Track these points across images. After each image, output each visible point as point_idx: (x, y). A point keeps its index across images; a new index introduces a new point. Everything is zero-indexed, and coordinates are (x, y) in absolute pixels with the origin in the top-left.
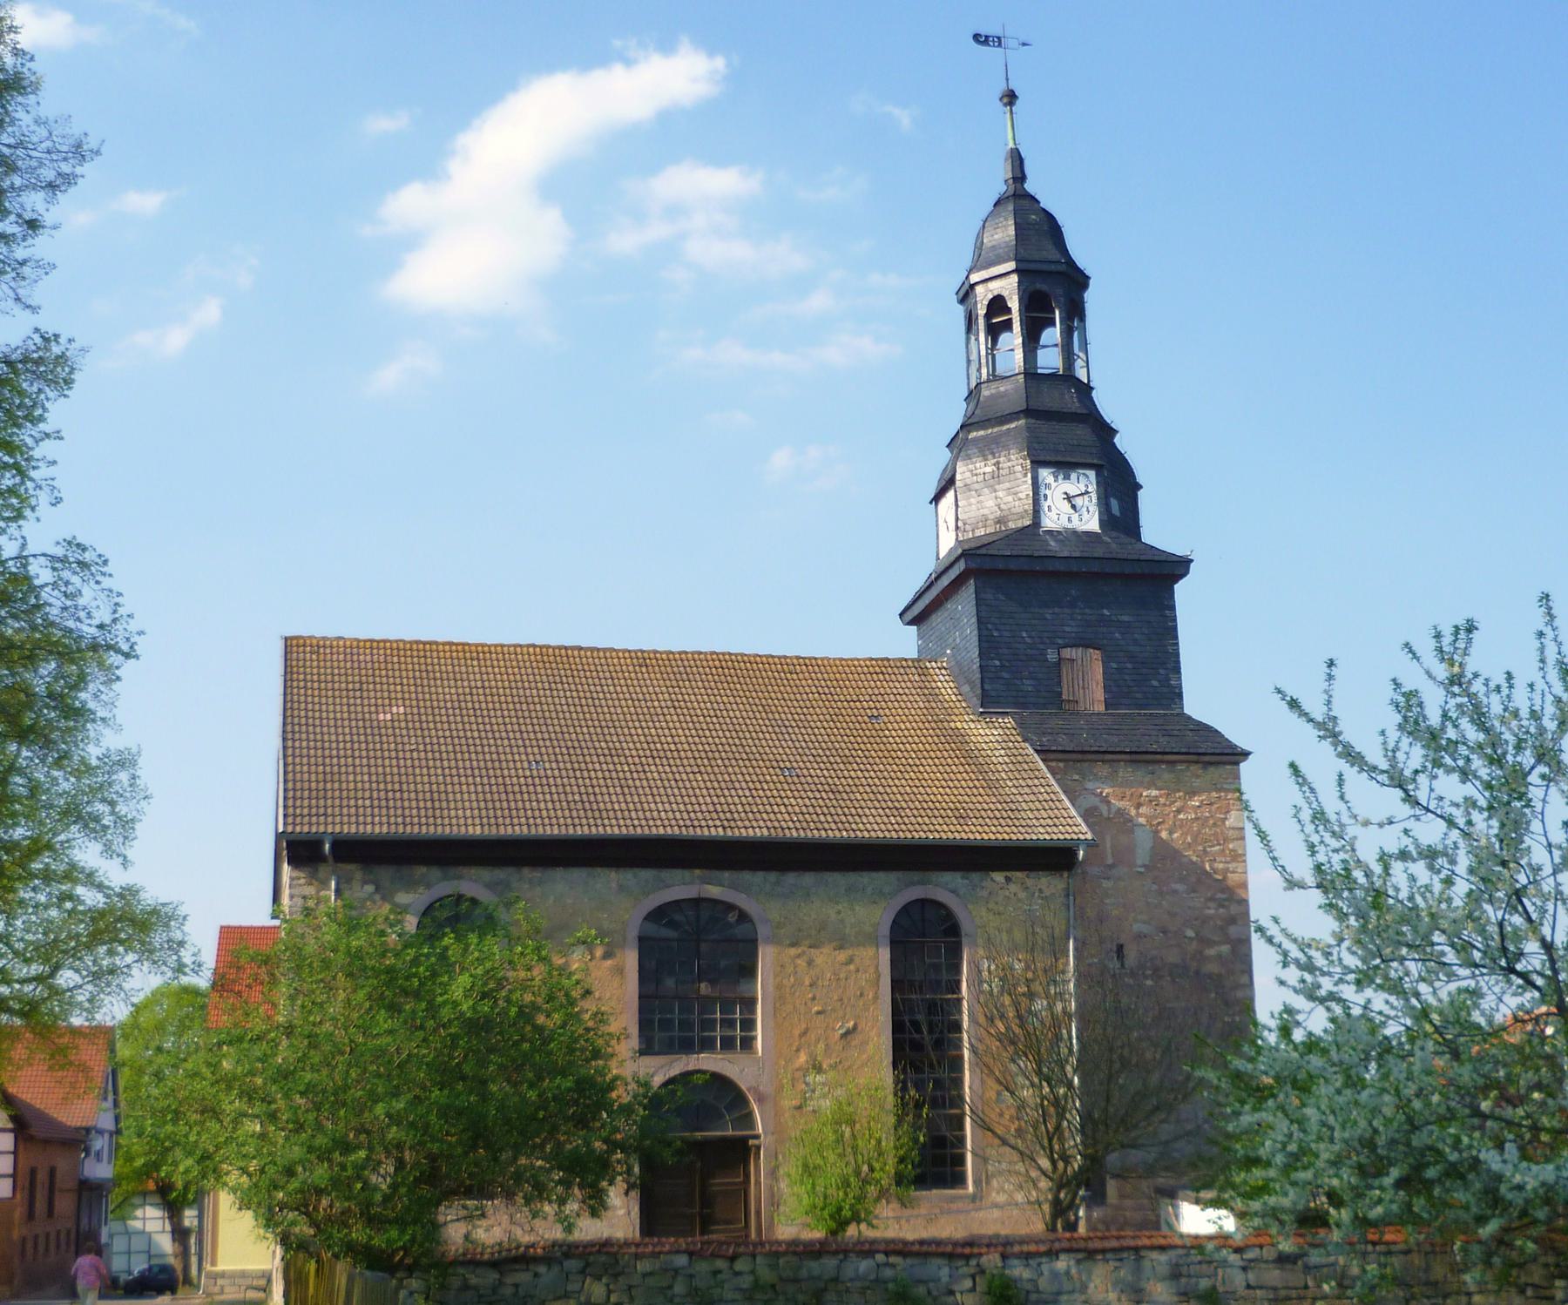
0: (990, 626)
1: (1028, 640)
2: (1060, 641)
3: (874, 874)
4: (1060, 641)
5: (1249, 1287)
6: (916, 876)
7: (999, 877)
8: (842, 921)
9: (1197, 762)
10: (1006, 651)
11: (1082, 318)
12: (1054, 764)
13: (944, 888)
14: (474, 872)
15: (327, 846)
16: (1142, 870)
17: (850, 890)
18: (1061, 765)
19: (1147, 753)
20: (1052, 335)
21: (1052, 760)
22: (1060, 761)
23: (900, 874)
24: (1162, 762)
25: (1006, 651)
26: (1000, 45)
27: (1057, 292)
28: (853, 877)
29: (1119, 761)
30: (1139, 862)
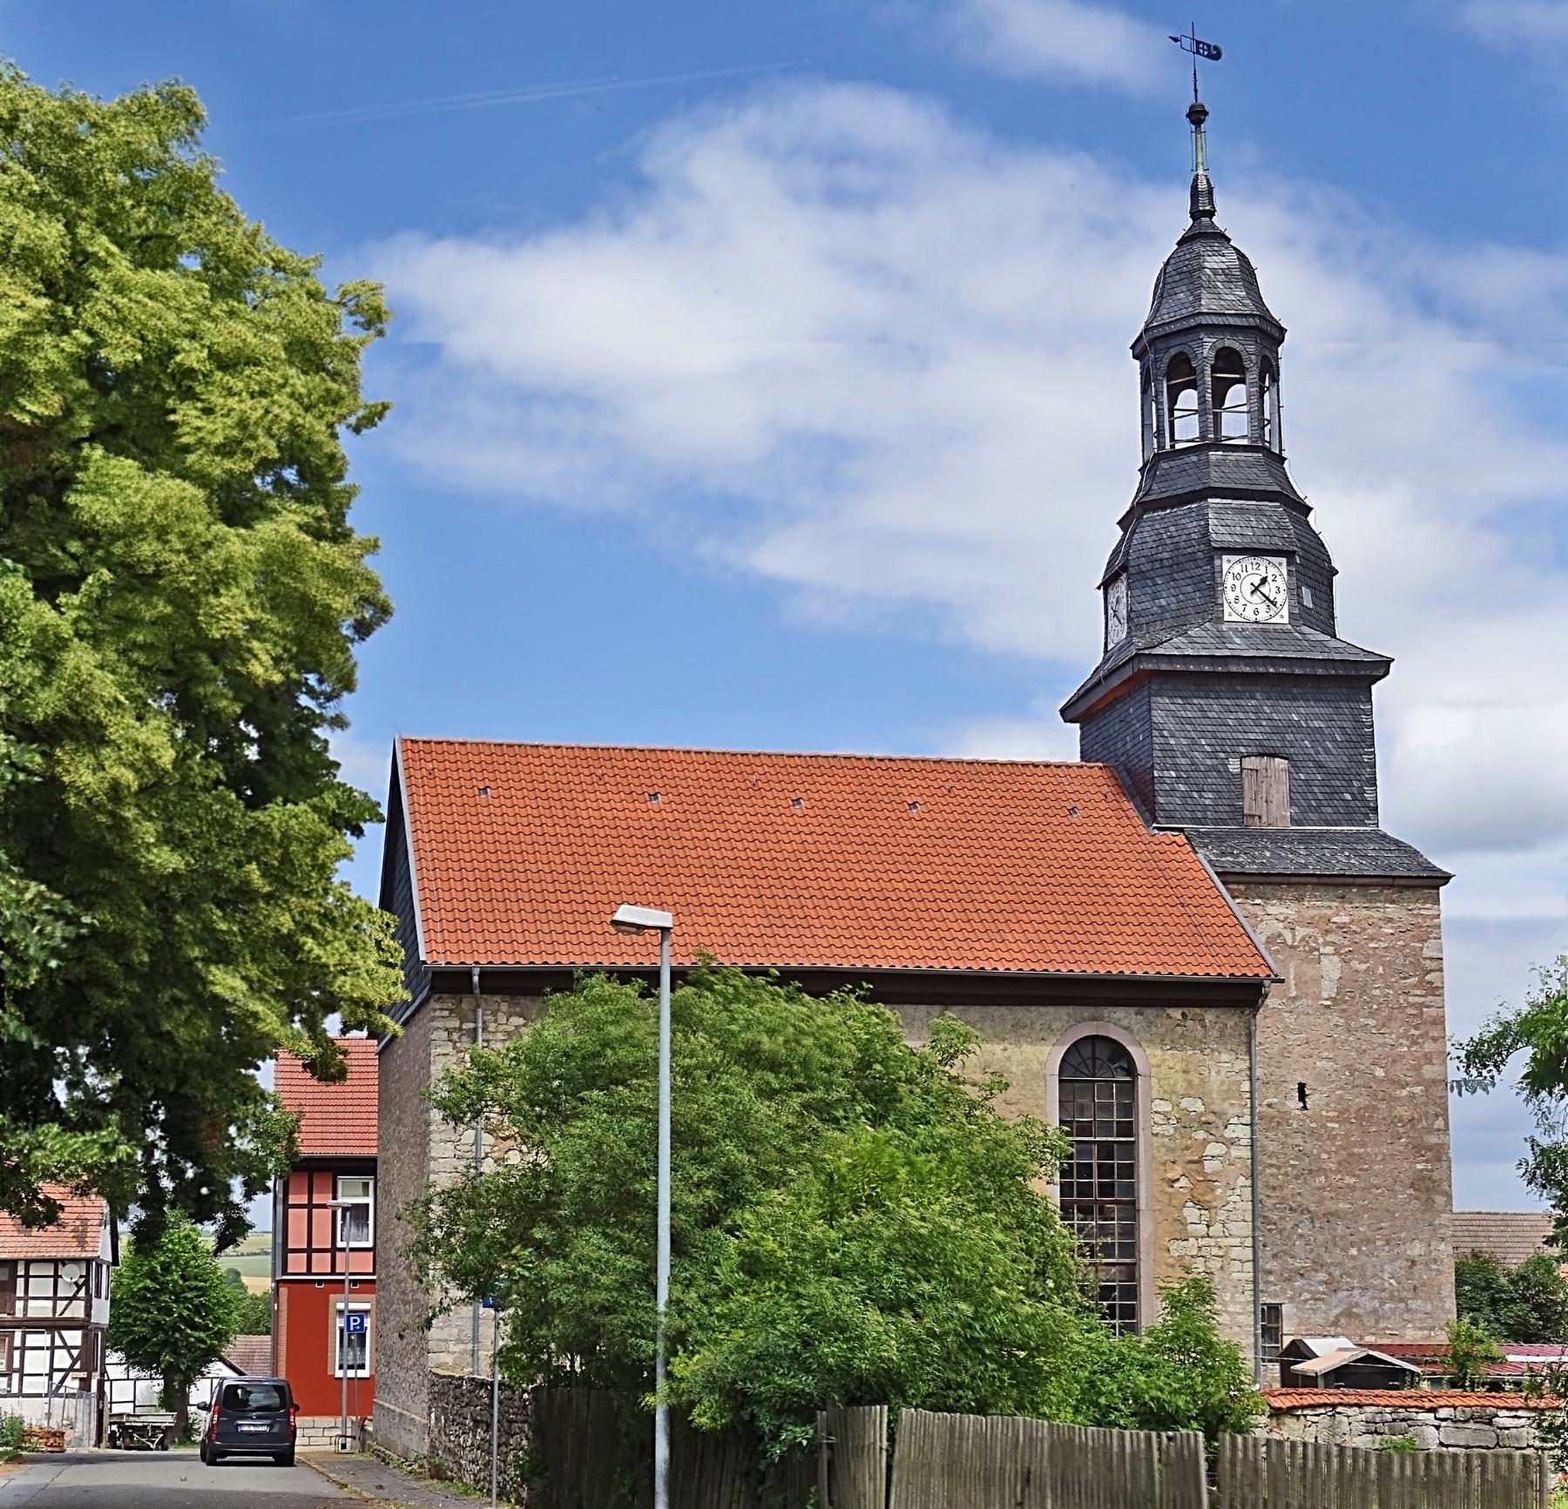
0: (1165, 733)
1: (1208, 749)
2: (1242, 749)
3: (1043, 1009)
4: (1242, 749)
5: (1441, 1444)
6: (1087, 1011)
7: (1176, 1013)
8: (1008, 1058)
9: (1392, 886)
10: (1183, 761)
11: (1275, 379)
12: (1235, 887)
13: (1119, 1024)
14: (1120, 1013)
15: (476, 979)
16: (1328, 1003)
17: (1017, 1026)
18: (1242, 887)
19: (1363, 876)
20: (1237, 394)
21: (1233, 883)
22: (1239, 883)
23: (1070, 1009)
24: (1354, 885)
25: (1183, 761)
26: (1198, 43)
27: (1248, 349)
28: (1020, 1012)
29: (1305, 884)
30: (1325, 995)
